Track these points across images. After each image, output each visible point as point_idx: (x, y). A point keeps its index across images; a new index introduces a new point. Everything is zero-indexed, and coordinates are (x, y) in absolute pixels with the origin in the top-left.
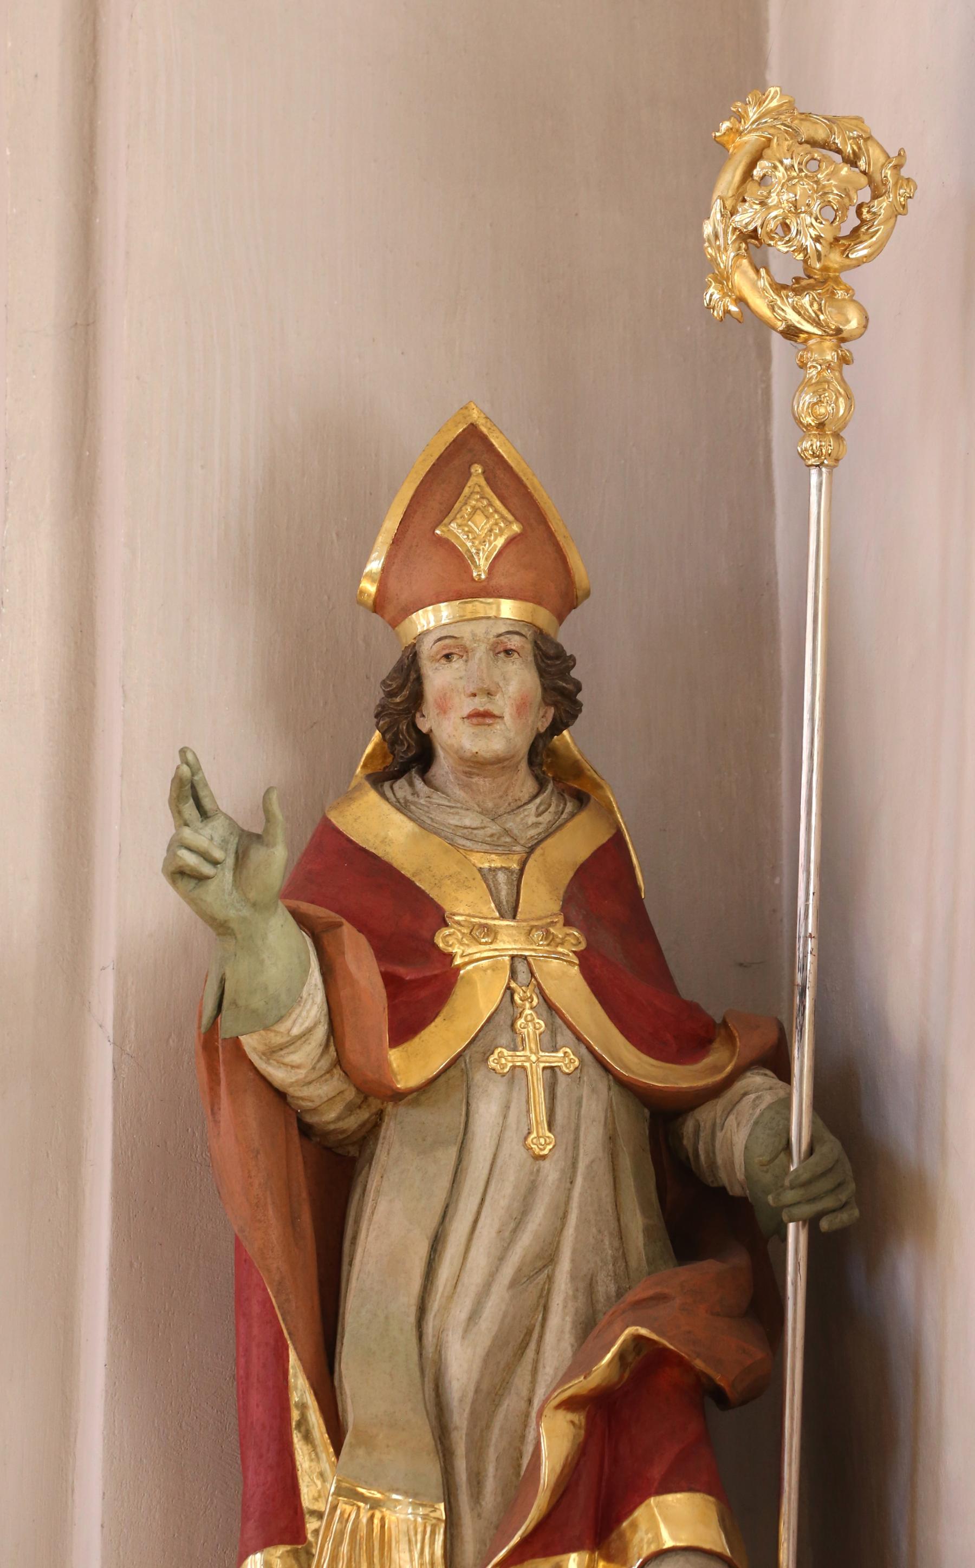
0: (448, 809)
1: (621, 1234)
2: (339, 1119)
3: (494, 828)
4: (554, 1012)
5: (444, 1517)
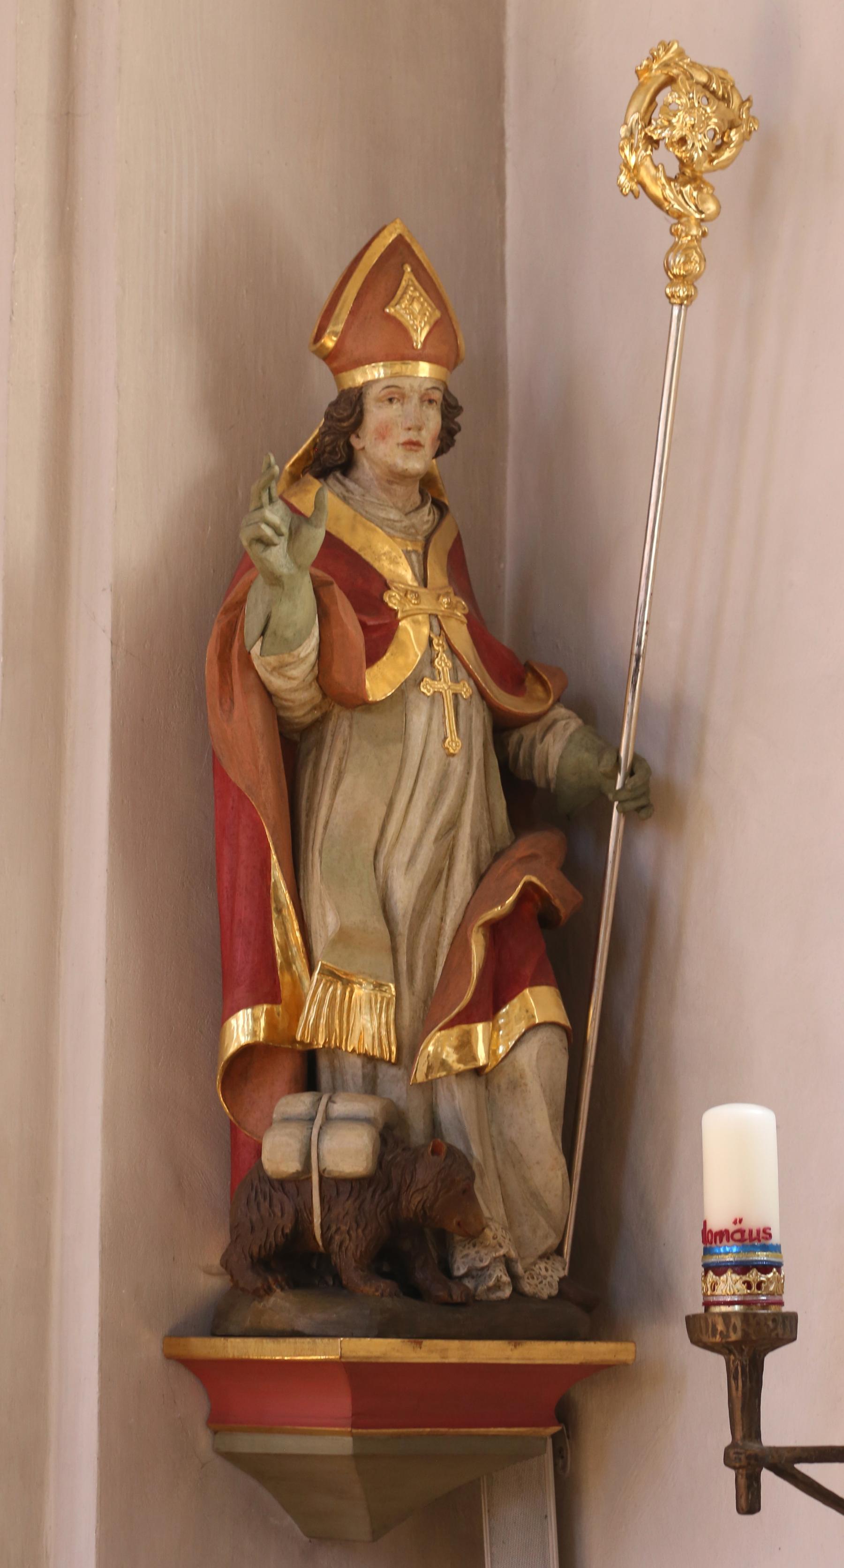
1: (490, 811)
2: (304, 715)
3: (406, 522)
4: (454, 655)
5: (394, 993)
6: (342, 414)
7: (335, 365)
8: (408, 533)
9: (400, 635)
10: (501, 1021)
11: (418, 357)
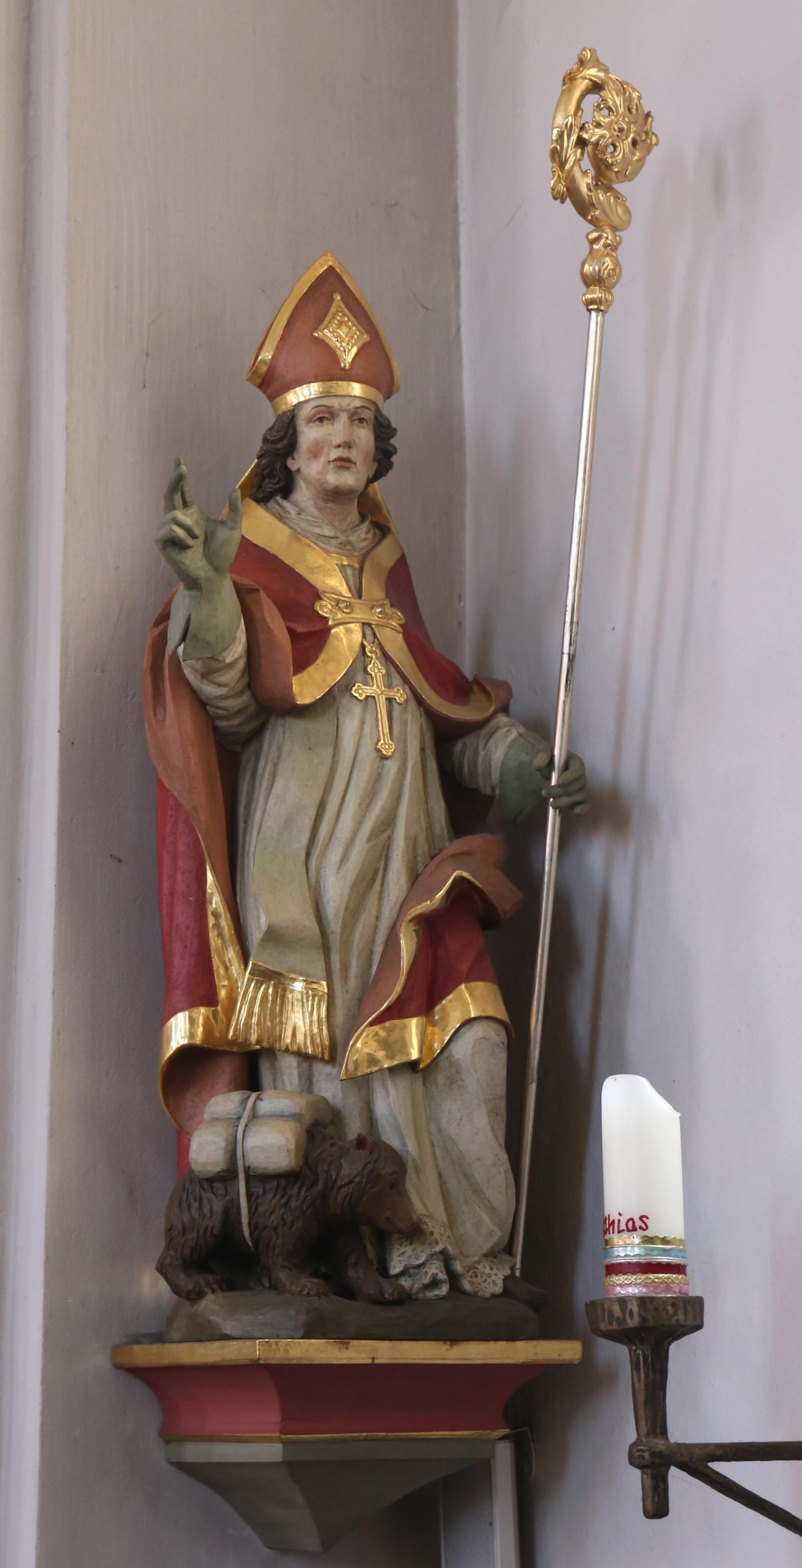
0: (314, 523)
1: (428, 814)
2: (239, 725)
3: (343, 538)
4: (389, 663)
5: (326, 991)
7: (270, 391)
8: (345, 547)
9: (332, 642)
10: (437, 1017)
11: (347, 376)
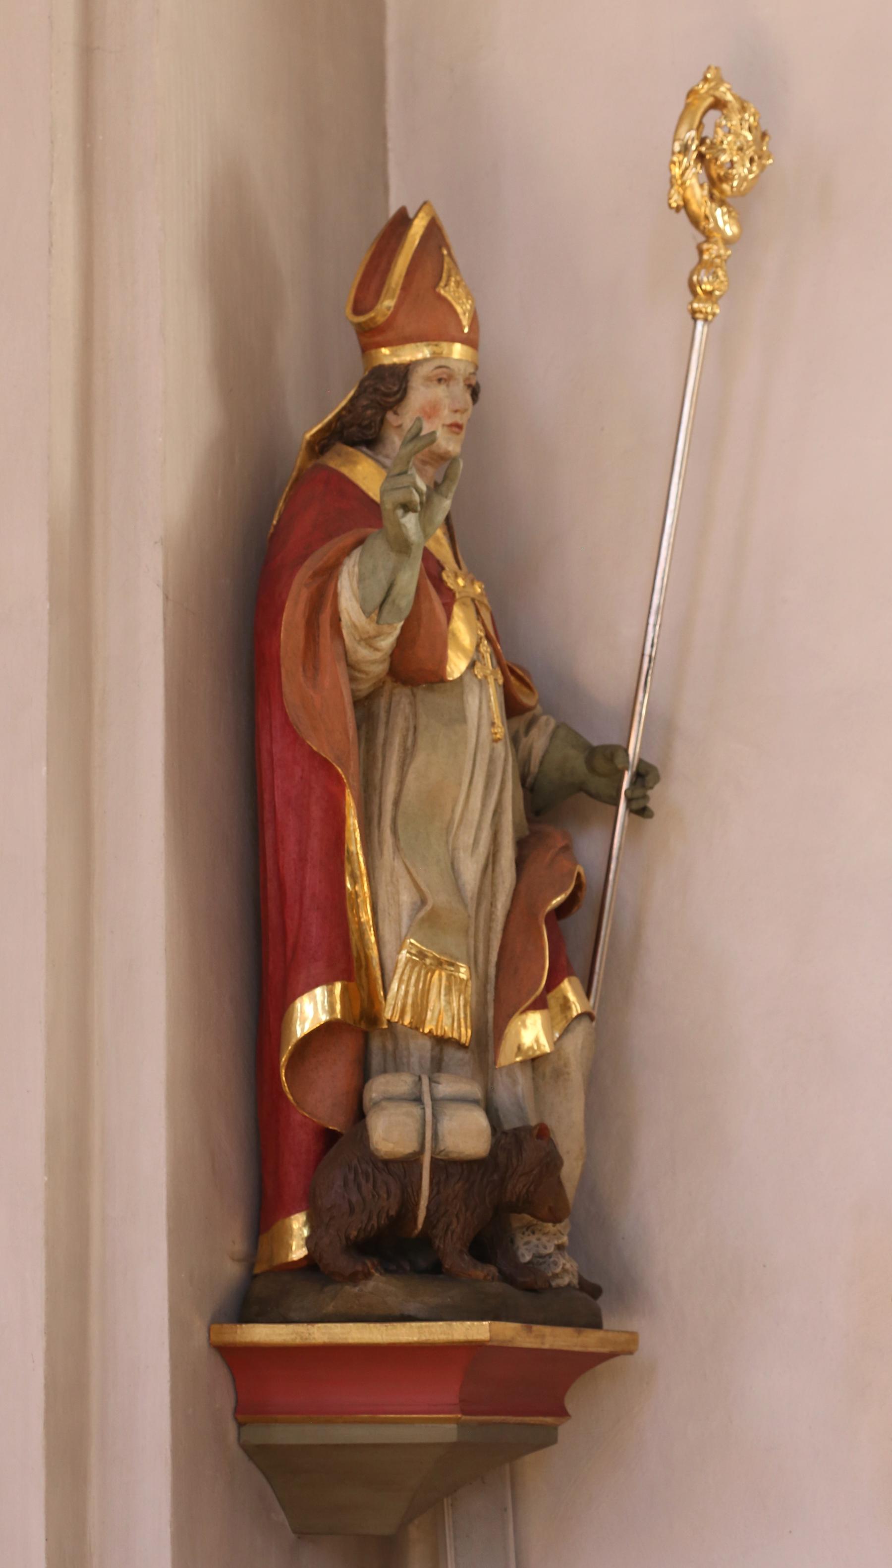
6: (390, 389)
